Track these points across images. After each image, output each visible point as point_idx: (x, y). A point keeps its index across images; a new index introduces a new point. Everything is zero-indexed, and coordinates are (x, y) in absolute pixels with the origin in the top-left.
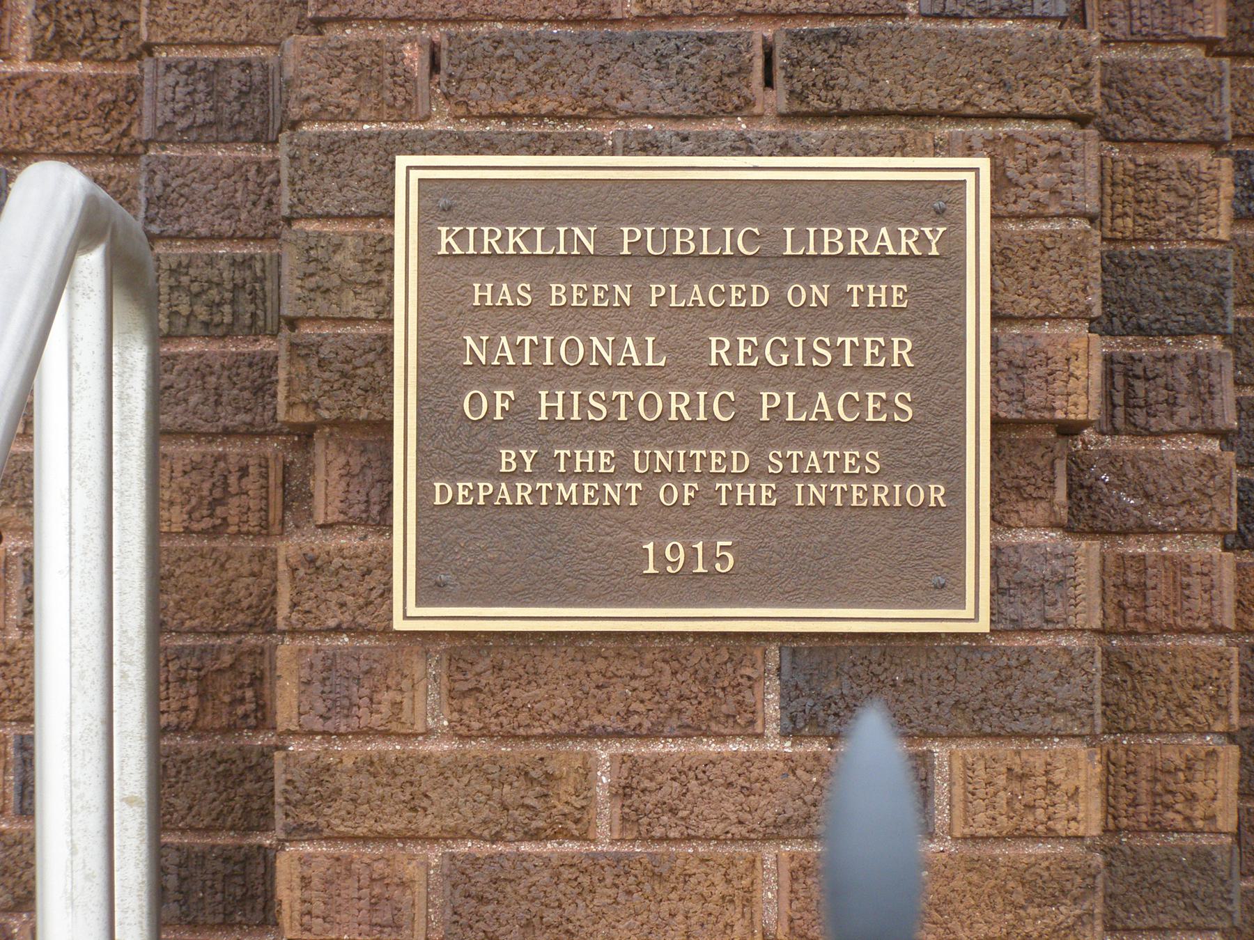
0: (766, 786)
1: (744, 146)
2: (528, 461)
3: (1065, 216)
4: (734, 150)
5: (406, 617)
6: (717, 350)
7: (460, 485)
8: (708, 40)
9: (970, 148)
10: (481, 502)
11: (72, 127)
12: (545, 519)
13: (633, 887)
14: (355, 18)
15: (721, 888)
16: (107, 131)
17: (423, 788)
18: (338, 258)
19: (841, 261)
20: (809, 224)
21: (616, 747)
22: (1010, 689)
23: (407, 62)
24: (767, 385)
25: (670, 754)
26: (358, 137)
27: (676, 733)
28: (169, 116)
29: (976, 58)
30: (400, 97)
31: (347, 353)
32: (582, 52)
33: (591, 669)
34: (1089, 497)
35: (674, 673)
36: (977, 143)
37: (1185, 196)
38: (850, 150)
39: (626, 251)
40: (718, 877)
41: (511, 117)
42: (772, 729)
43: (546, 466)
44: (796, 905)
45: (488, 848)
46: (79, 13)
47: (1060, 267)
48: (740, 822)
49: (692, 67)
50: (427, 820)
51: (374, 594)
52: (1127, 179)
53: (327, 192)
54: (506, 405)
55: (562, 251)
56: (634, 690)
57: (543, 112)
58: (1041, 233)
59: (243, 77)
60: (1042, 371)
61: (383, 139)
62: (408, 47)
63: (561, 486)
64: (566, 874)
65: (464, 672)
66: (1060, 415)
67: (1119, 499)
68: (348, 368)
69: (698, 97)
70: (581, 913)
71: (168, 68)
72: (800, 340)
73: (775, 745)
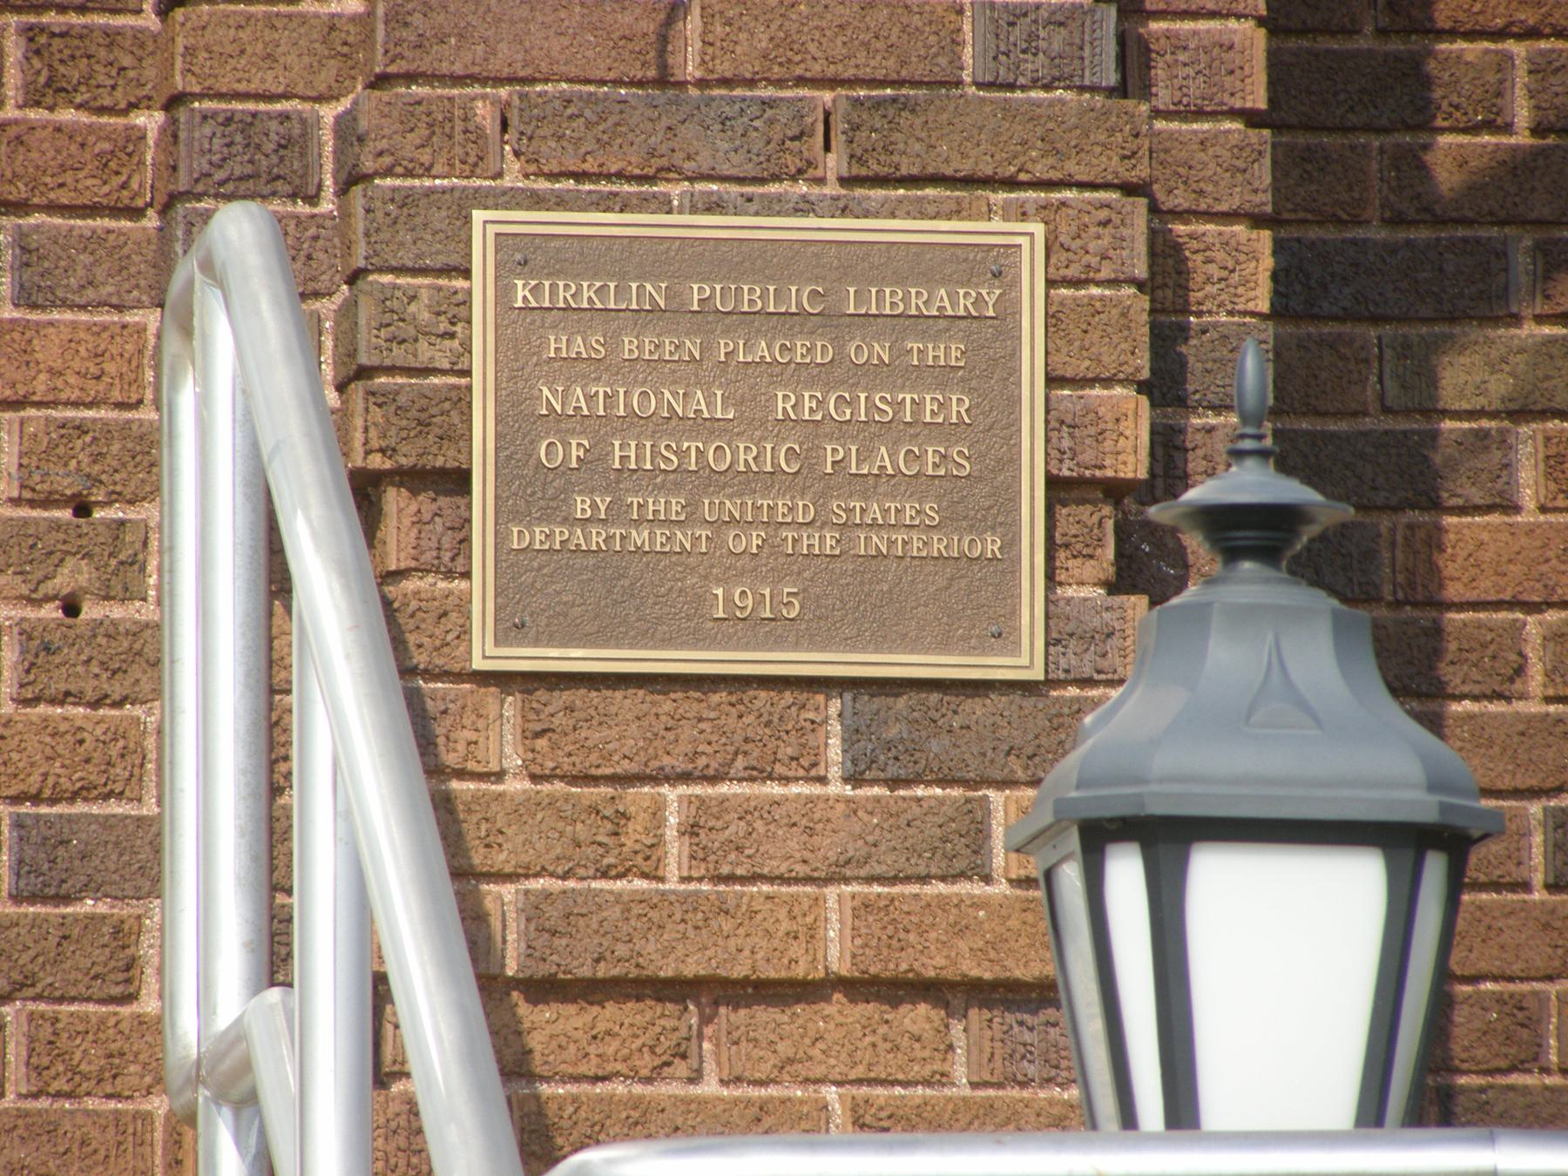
0: (829, 827)
1: (805, 207)
2: (603, 508)
3: (1113, 283)
4: (797, 211)
5: (485, 657)
6: (783, 404)
7: (537, 530)
8: (766, 103)
9: (1024, 214)
10: (557, 547)
11: (68, 177)
12: (609, 566)
13: (700, 924)
14: (423, 75)
15: (785, 925)
16: (105, 183)
17: (499, 825)
18: (413, 308)
19: (902, 320)
20: (871, 283)
21: (683, 789)
22: (1063, 736)
23: (478, 119)
24: (830, 437)
25: (735, 795)
26: (430, 192)
27: (741, 775)
28: (206, 167)
29: (1030, 126)
30: (473, 153)
31: (424, 402)
32: (649, 113)
33: (660, 711)
34: (1129, 567)
35: (740, 717)
36: (1031, 209)
37: (1225, 268)
38: (908, 213)
39: (696, 308)
40: (782, 914)
41: (580, 176)
42: (835, 772)
43: (617, 514)
44: (858, 942)
45: (556, 885)
46: (73, 57)
47: (1110, 330)
48: (805, 862)
49: (756, 129)
50: (502, 857)
51: (449, 637)
52: (1167, 250)
53: (402, 244)
54: (581, 454)
55: (634, 306)
56: (701, 732)
57: (613, 170)
58: (1092, 298)
59: (282, 130)
60: (1092, 431)
61: (457, 194)
62: (480, 104)
63: (634, 533)
64: (637, 909)
65: (538, 713)
66: (1110, 473)
67: (1160, 568)
68: (423, 416)
69: (762, 159)
70: (651, 947)
71: (205, 118)
72: (863, 396)
73: (836, 788)
